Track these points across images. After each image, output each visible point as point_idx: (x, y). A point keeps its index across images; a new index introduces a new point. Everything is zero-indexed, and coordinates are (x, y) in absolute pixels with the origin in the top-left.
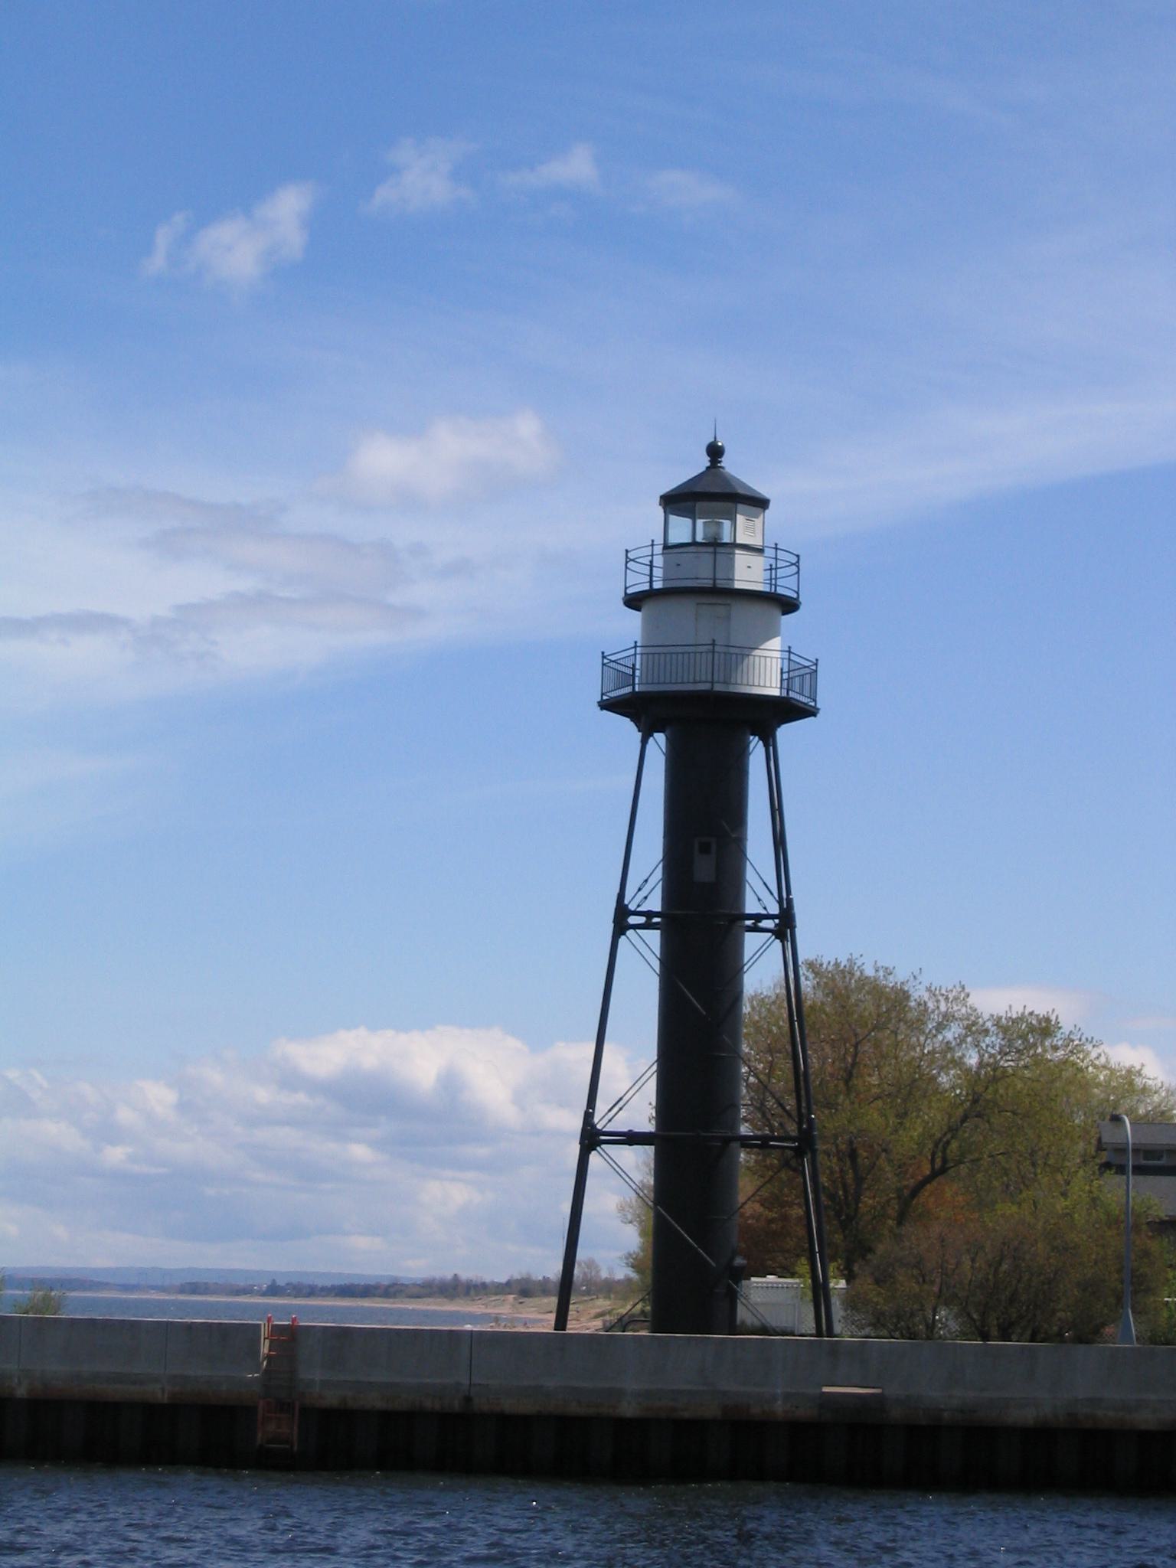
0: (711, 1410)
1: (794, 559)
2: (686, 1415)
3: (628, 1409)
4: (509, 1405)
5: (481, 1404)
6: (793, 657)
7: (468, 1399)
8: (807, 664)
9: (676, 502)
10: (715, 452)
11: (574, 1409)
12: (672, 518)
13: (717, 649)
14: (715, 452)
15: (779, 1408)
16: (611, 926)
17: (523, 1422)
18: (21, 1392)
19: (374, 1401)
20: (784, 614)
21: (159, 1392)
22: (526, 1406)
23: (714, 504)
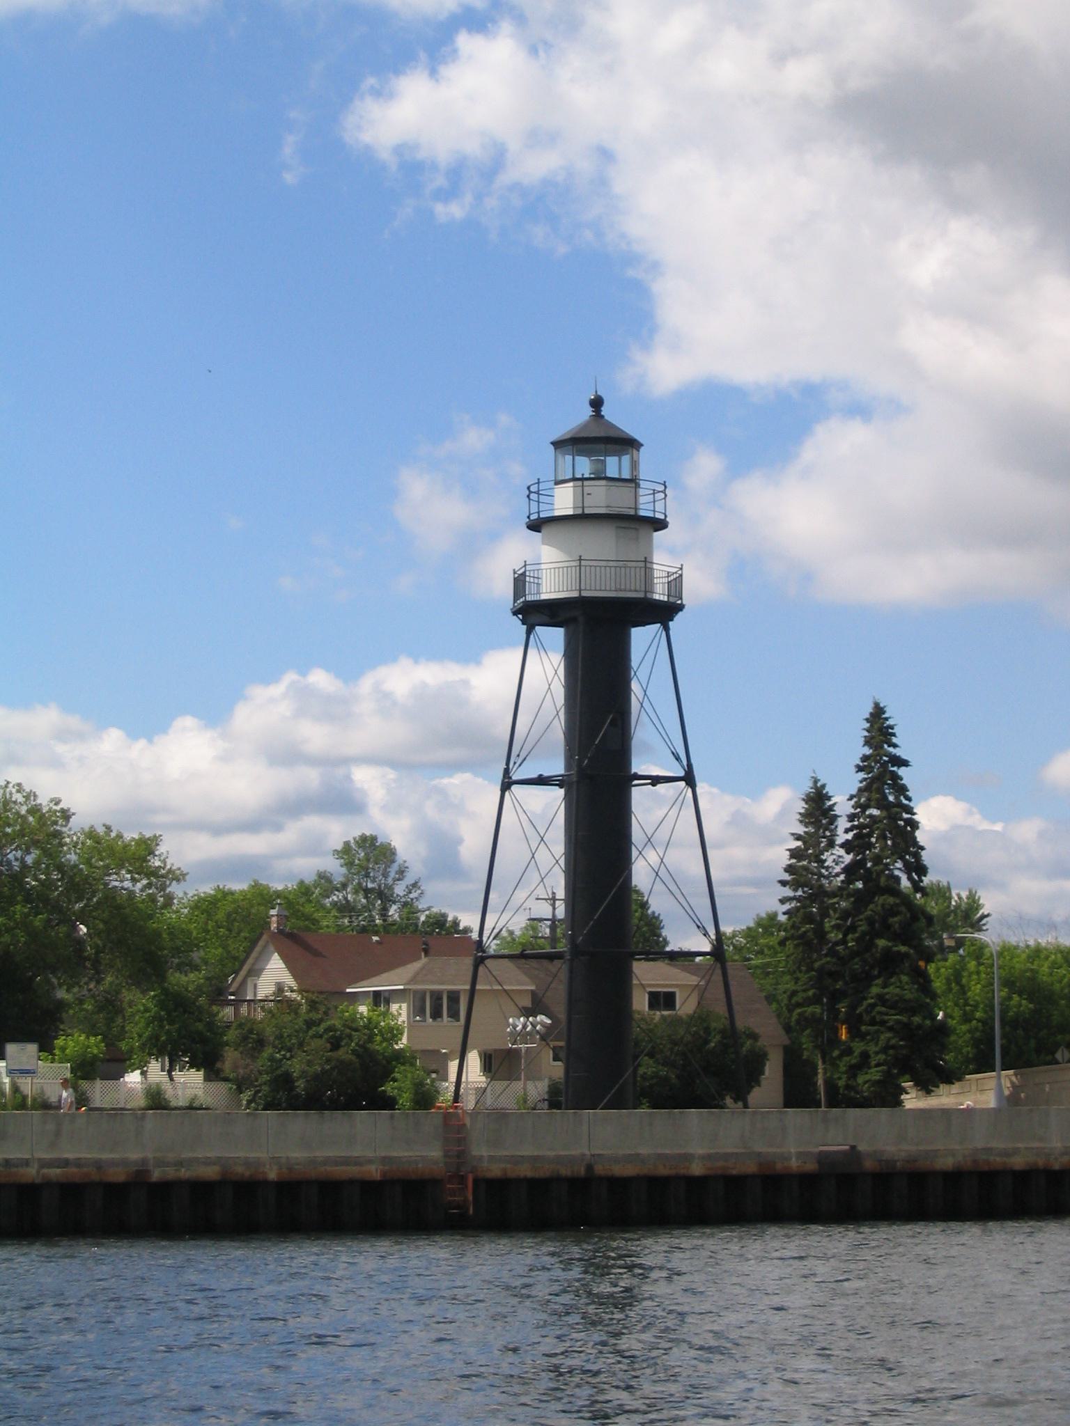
0: (751, 1168)
1: (662, 488)
2: (734, 1172)
3: (697, 1169)
4: (619, 1170)
5: (599, 1170)
7: (590, 1168)
8: (674, 570)
9: (573, 444)
10: (597, 403)
11: (663, 1171)
12: (577, 458)
14: (597, 403)
15: (794, 1164)
16: (695, 773)
17: (165, 1187)
18: (272, 1175)
19: (525, 1171)
20: (656, 530)
21: (374, 1172)
22: (629, 1171)
23: (590, 446)
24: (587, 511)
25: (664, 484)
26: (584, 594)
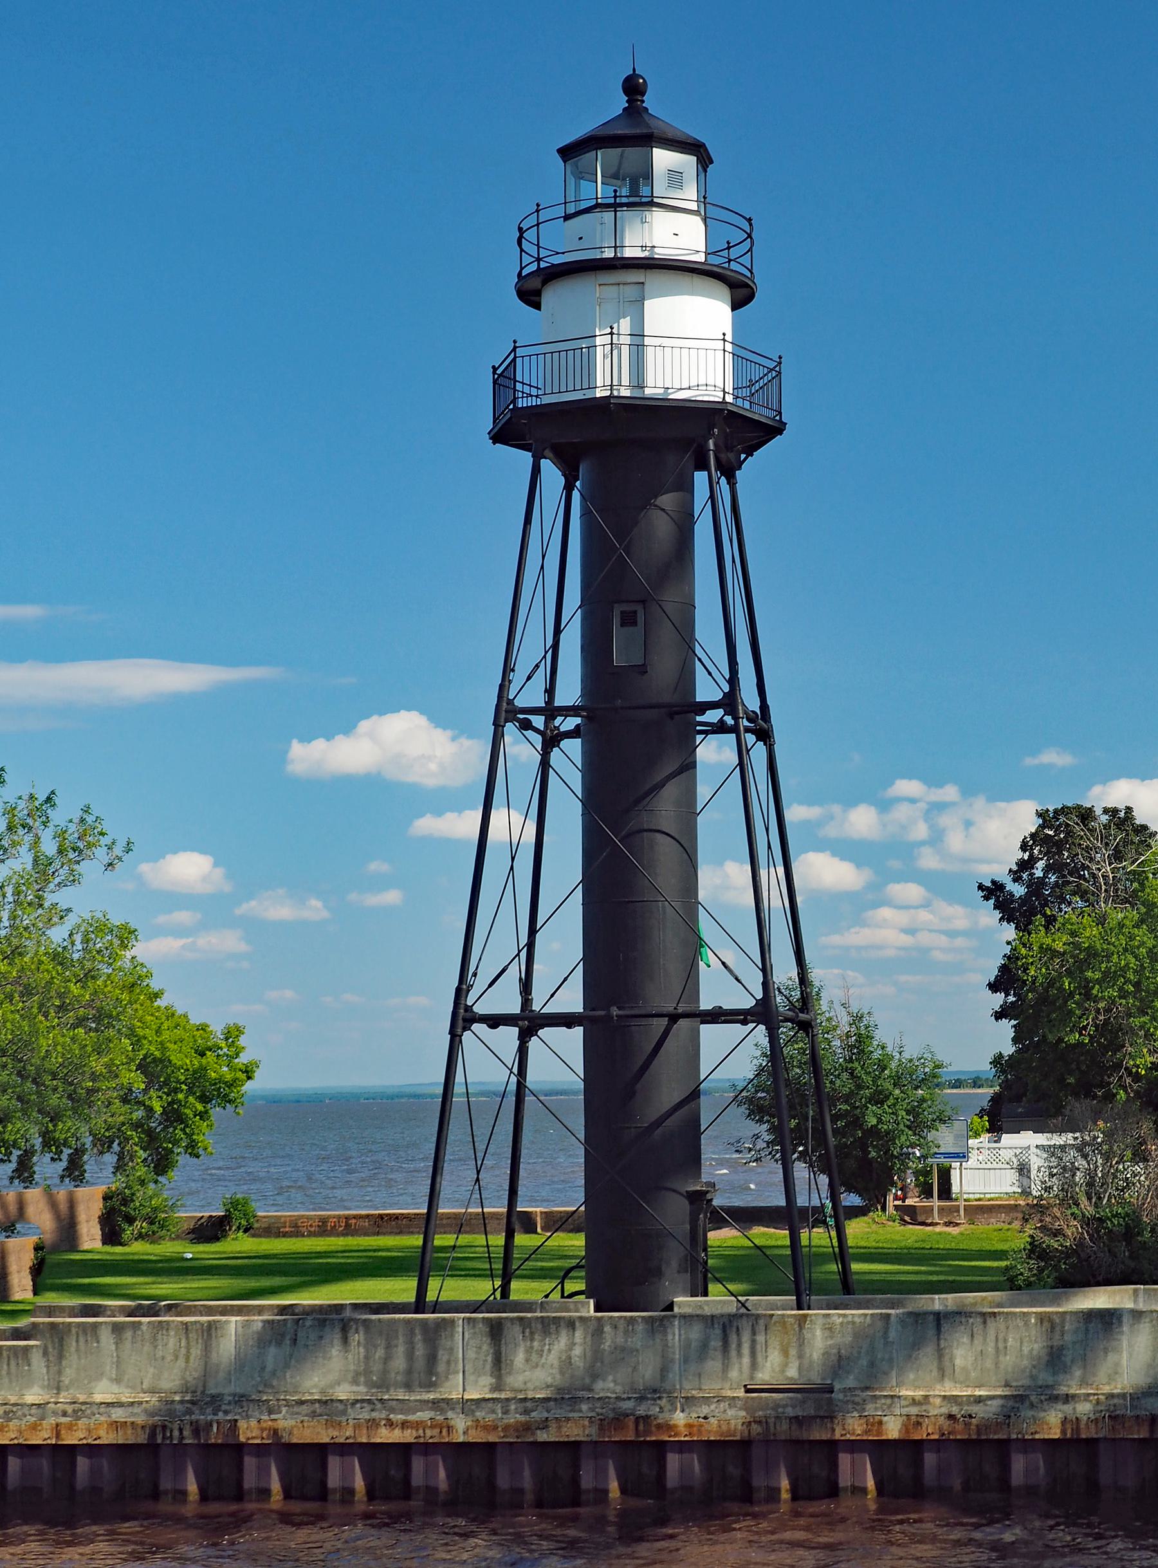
8: (772, 365)
10: (633, 88)
14: (633, 88)
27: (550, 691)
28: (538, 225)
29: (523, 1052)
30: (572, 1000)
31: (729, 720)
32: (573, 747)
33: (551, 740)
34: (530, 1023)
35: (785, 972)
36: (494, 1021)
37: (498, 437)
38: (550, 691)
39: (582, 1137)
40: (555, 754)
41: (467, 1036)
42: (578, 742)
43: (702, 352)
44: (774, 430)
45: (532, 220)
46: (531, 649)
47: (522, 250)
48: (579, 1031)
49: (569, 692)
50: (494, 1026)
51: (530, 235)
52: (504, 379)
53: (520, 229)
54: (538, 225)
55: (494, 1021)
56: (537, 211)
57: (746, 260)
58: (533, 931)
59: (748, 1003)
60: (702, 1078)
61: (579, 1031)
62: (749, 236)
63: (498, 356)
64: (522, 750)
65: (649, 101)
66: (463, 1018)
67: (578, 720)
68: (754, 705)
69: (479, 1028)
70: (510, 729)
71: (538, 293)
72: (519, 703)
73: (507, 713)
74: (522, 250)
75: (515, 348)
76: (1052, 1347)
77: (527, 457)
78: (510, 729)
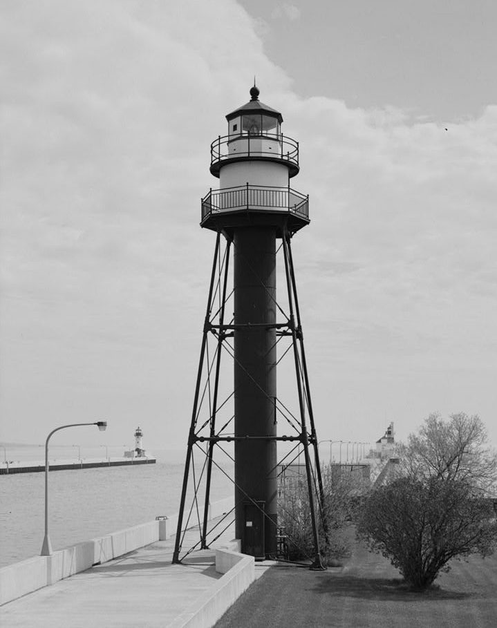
6: (291, 191)
8: (305, 198)
10: (255, 93)
13: (249, 188)
14: (255, 93)
24: (251, 155)
25: (298, 143)
26: (250, 207)
27: (221, 320)
28: (219, 144)
29: (211, 450)
30: (230, 431)
31: (290, 331)
32: (231, 340)
33: (222, 338)
34: (213, 440)
35: (309, 430)
36: (202, 439)
37: (203, 225)
38: (221, 320)
39: (234, 480)
40: (223, 342)
41: (194, 446)
42: (233, 338)
43: (278, 205)
44: (306, 223)
45: (217, 142)
46: (216, 307)
47: (212, 155)
48: (233, 443)
49: (229, 318)
50: (202, 441)
51: (216, 149)
52: (206, 204)
53: (212, 146)
54: (219, 144)
55: (202, 439)
56: (219, 139)
57: (296, 158)
58: (214, 412)
59: (297, 435)
60: (268, 568)
61: (233, 443)
62: (297, 149)
63: (204, 195)
64: (213, 339)
65: (260, 97)
66: (193, 439)
67: (233, 330)
68: (296, 325)
69: (198, 442)
70: (209, 333)
71: (219, 171)
72: (213, 324)
73: (208, 327)
74: (212, 155)
75: (211, 191)
76: (451, 492)
77: (216, 233)
78: (209, 333)
